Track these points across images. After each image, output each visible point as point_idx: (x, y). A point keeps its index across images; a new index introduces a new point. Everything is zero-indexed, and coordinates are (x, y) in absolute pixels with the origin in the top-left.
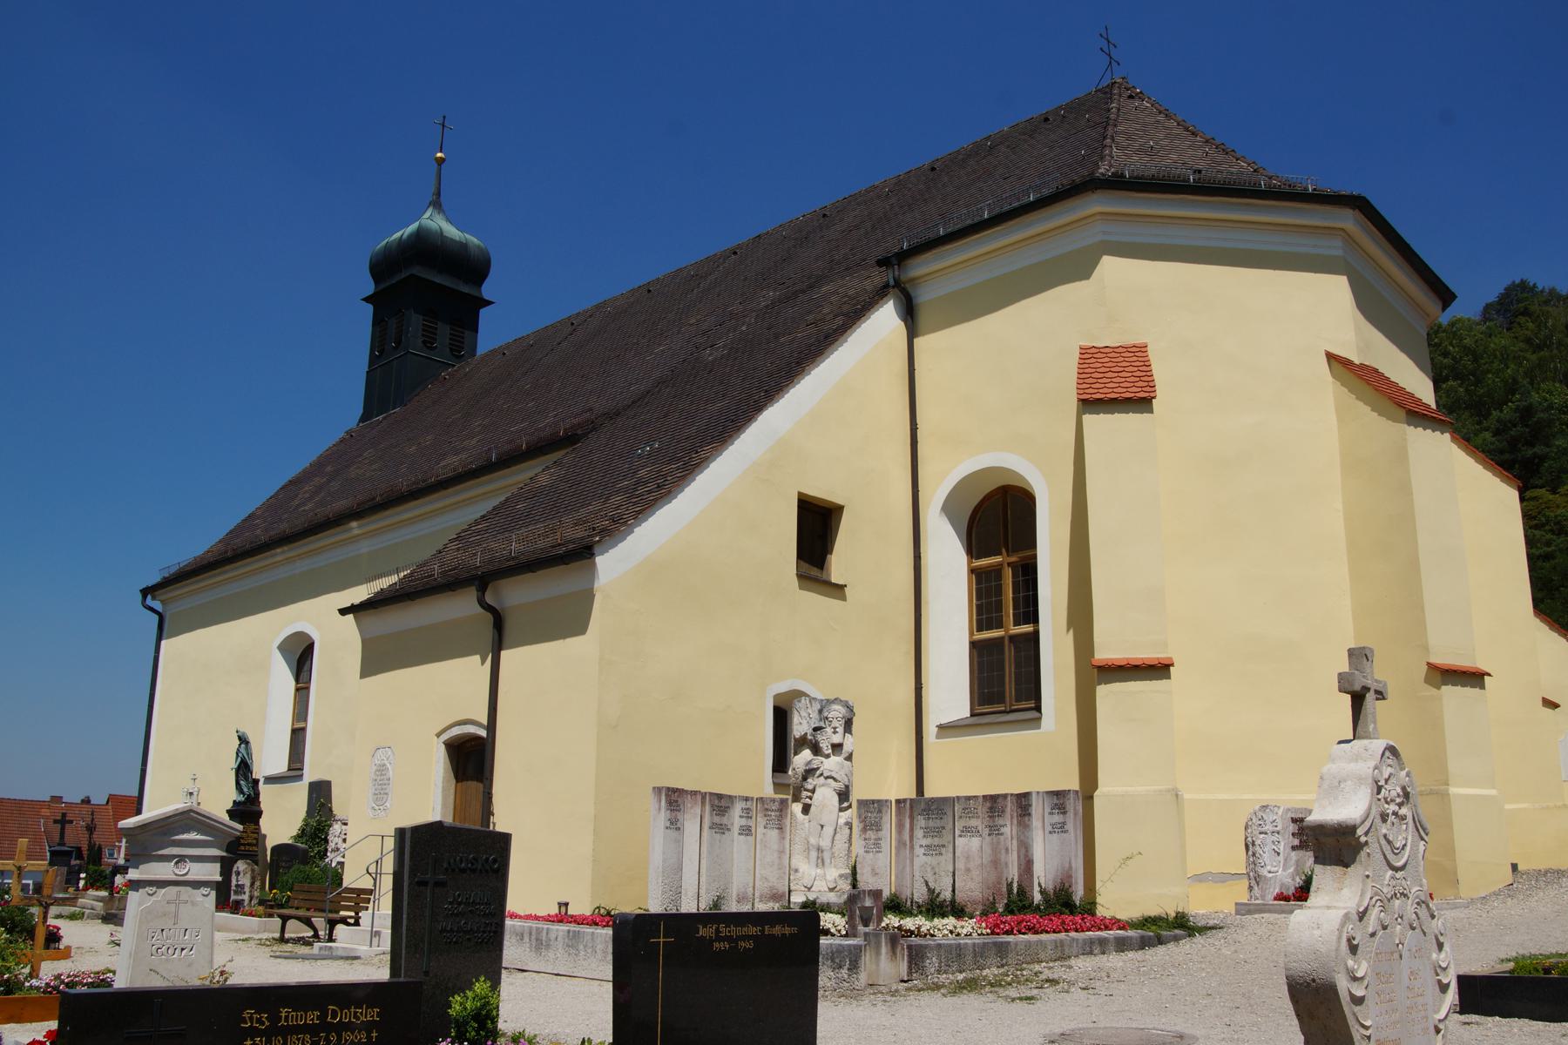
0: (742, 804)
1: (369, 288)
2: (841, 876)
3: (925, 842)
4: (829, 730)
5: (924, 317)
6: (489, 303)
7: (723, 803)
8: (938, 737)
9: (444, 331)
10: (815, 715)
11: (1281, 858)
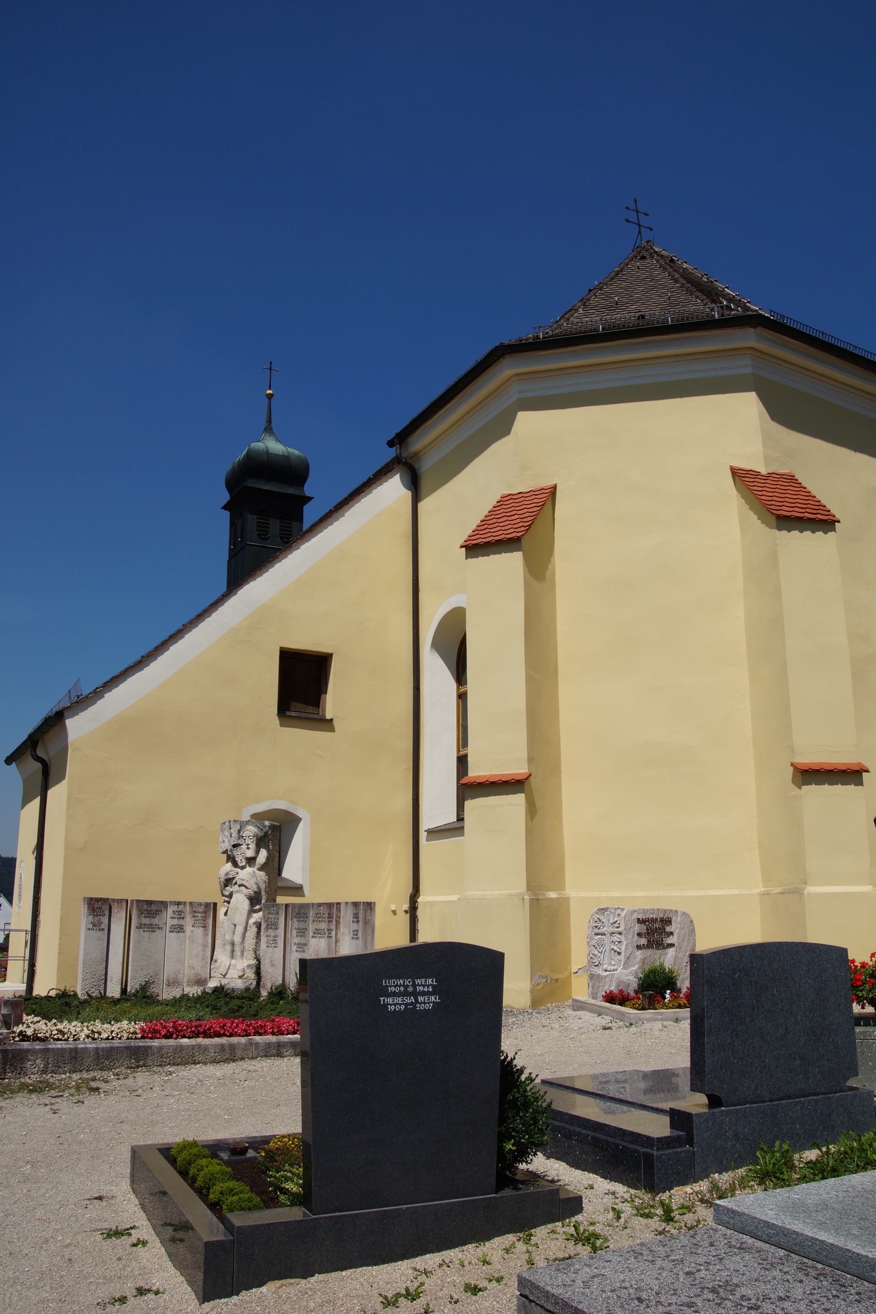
0: (175, 908)
1: (226, 497)
2: (248, 966)
3: (297, 940)
4: (244, 847)
5: (424, 484)
7: (154, 908)
8: (427, 841)
9: (275, 526)
10: (235, 835)
11: (622, 957)
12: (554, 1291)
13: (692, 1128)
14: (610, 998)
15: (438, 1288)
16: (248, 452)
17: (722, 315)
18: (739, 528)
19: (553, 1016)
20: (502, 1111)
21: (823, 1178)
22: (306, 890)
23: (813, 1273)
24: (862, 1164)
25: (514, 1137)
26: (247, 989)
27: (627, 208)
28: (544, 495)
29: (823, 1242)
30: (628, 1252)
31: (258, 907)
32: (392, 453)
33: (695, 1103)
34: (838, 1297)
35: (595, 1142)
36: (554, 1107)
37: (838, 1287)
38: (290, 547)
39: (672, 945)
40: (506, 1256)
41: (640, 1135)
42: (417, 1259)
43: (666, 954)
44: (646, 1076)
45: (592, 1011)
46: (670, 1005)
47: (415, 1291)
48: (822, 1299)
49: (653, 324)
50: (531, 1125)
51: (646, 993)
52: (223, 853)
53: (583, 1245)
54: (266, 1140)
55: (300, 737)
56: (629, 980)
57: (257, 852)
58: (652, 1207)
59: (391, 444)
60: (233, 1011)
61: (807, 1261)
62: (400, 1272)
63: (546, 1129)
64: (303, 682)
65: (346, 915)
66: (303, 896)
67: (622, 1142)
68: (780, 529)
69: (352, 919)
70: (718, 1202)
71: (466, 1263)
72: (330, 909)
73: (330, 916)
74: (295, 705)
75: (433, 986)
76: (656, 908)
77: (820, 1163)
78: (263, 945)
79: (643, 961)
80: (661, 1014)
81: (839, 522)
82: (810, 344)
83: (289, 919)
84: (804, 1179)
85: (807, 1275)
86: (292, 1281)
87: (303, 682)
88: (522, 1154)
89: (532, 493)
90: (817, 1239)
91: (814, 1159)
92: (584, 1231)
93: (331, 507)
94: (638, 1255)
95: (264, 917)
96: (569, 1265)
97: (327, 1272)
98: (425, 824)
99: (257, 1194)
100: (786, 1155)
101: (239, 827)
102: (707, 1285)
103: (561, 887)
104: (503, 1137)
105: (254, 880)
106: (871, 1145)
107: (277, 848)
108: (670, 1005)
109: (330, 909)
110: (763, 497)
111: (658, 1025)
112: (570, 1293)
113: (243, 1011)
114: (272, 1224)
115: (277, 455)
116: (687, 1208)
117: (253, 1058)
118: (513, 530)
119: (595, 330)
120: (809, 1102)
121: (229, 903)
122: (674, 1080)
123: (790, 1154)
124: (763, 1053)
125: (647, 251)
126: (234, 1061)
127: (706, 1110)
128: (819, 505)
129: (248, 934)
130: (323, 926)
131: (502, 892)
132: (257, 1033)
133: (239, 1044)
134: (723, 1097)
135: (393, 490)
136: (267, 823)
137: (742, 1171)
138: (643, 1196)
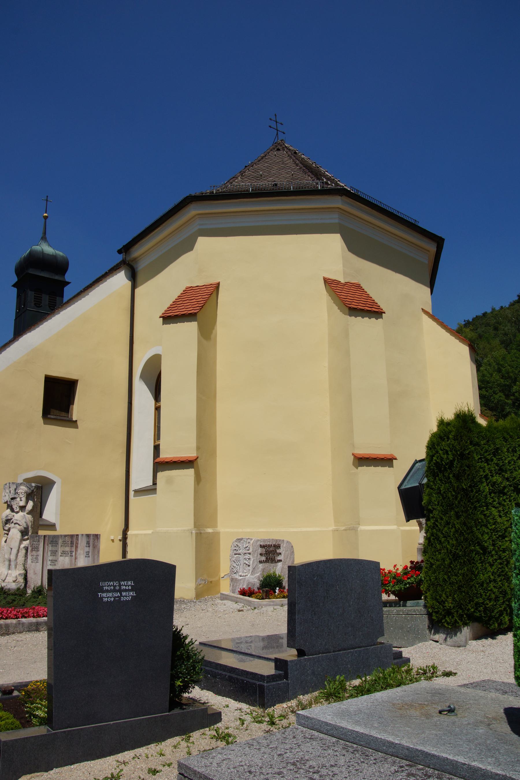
1: (15, 279)
2: (19, 574)
4: (18, 499)
5: (140, 277)
6: (68, 283)
8: (134, 496)
9: (45, 299)
11: (251, 568)
12: (199, 770)
13: (288, 669)
14: (243, 593)
15: (131, 772)
16: (30, 253)
17: (323, 187)
18: (327, 314)
19: (209, 604)
20: (173, 661)
21: (362, 695)
22: (58, 527)
23: (351, 750)
24: (384, 687)
25: (181, 677)
26: (18, 589)
27: (271, 119)
28: (212, 288)
29: (357, 732)
30: (245, 744)
31: (26, 537)
32: (120, 258)
33: (289, 654)
34: (363, 762)
35: (230, 679)
36: (205, 658)
37: (364, 757)
38: (54, 313)
39: (280, 561)
40: (174, 750)
41: (257, 674)
42: (119, 755)
43: (276, 566)
44: (263, 639)
45: (232, 601)
46: (279, 596)
47: (117, 775)
48: (355, 764)
49: (282, 189)
50: (191, 670)
51: (264, 589)
52: (5, 503)
53: (222, 741)
54: (26, 684)
55: (57, 432)
56: (254, 581)
57: (27, 503)
58: (263, 716)
59: (120, 252)
60: (9, 603)
61: (348, 743)
62: (108, 763)
63: (201, 672)
64: (59, 397)
65: (82, 542)
66: (56, 530)
67: (246, 679)
68: (350, 316)
69: (85, 545)
70: (299, 712)
71: (150, 756)
72: (72, 539)
73: (72, 543)
74: (53, 411)
75: (131, 586)
76: (271, 538)
77: (361, 687)
78: (29, 561)
79: (263, 570)
80: (273, 602)
81: (384, 313)
82: (372, 208)
83: (46, 547)
84: (351, 696)
85: (348, 751)
86: (38, 774)
87: (59, 397)
88: (186, 688)
89: (192, 288)
90: (354, 731)
91: (358, 685)
92: (222, 732)
93: (81, 289)
94: (250, 745)
95: (30, 543)
96: (209, 754)
97: (61, 766)
98: (133, 486)
99: (17, 719)
100: (342, 683)
101: (15, 487)
102: (290, 761)
103: (215, 525)
104: (174, 678)
105: (24, 520)
106: (390, 675)
107: (40, 500)
108: (279, 596)
109: (72, 539)
110: (341, 296)
111: (271, 608)
112: (209, 771)
113: (15, 603)
114: (27, 738)
115: (48, 255)
116: (283, 716)
117: (20, 632)
118: (192, 309)
119: (247, 191)
120: (356, 652)
121: (8, 534)
122: (281, 641)
123: (344, 682)
124: (330, 624)
125: (281, 146)
126: (8, 634)
127: (296, 658)
128: (374, 302)
129: (20, 554)
130: (67, 549)
131: (179, 528)
132: (24, 617)
133: (11, 623)
134: (306, 650)
135: (120, 280)
136: (33, 485)
137: (316, 693)
138: (258, 710)
